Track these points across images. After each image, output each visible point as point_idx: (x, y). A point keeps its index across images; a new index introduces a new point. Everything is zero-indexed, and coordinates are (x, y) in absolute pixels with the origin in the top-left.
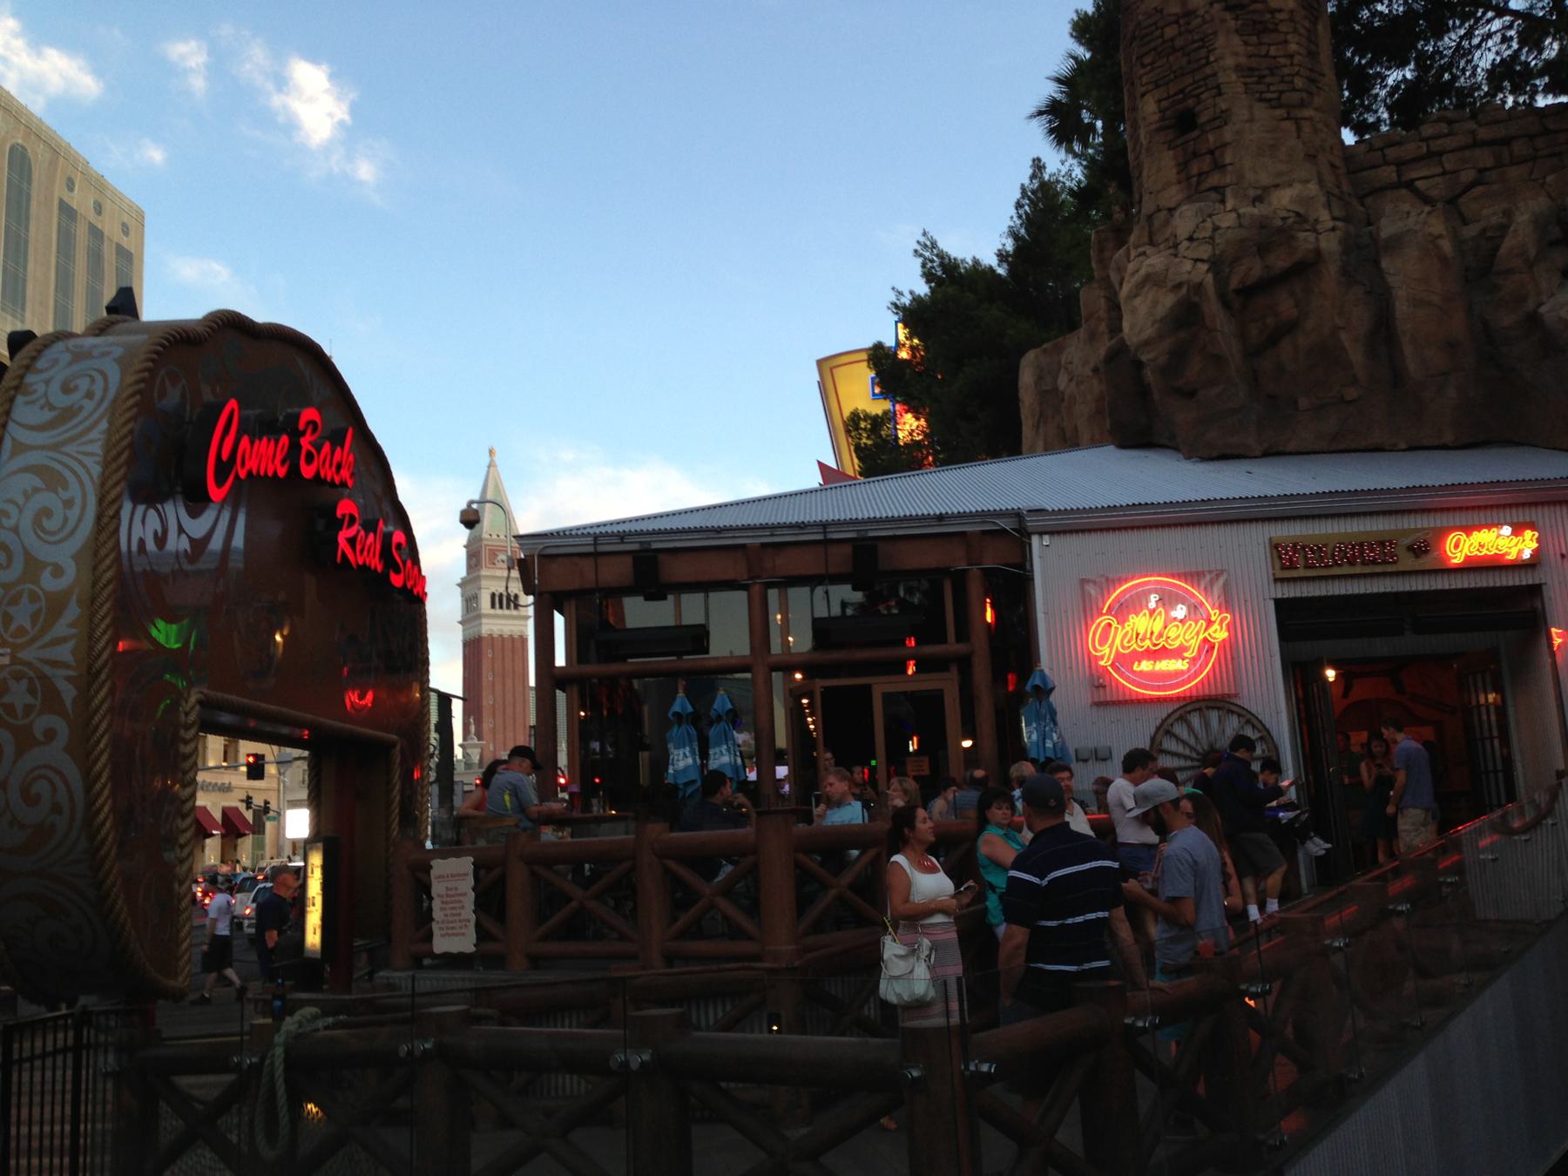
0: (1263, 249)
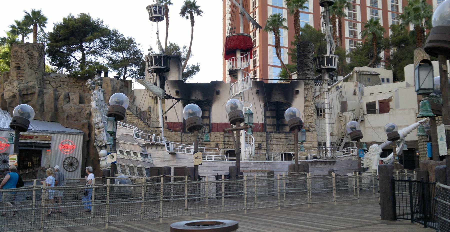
0: (27, 90)
